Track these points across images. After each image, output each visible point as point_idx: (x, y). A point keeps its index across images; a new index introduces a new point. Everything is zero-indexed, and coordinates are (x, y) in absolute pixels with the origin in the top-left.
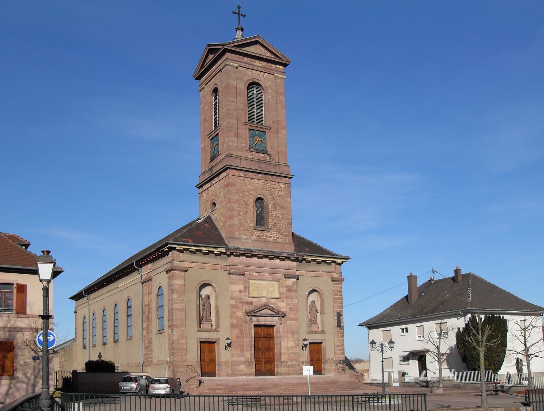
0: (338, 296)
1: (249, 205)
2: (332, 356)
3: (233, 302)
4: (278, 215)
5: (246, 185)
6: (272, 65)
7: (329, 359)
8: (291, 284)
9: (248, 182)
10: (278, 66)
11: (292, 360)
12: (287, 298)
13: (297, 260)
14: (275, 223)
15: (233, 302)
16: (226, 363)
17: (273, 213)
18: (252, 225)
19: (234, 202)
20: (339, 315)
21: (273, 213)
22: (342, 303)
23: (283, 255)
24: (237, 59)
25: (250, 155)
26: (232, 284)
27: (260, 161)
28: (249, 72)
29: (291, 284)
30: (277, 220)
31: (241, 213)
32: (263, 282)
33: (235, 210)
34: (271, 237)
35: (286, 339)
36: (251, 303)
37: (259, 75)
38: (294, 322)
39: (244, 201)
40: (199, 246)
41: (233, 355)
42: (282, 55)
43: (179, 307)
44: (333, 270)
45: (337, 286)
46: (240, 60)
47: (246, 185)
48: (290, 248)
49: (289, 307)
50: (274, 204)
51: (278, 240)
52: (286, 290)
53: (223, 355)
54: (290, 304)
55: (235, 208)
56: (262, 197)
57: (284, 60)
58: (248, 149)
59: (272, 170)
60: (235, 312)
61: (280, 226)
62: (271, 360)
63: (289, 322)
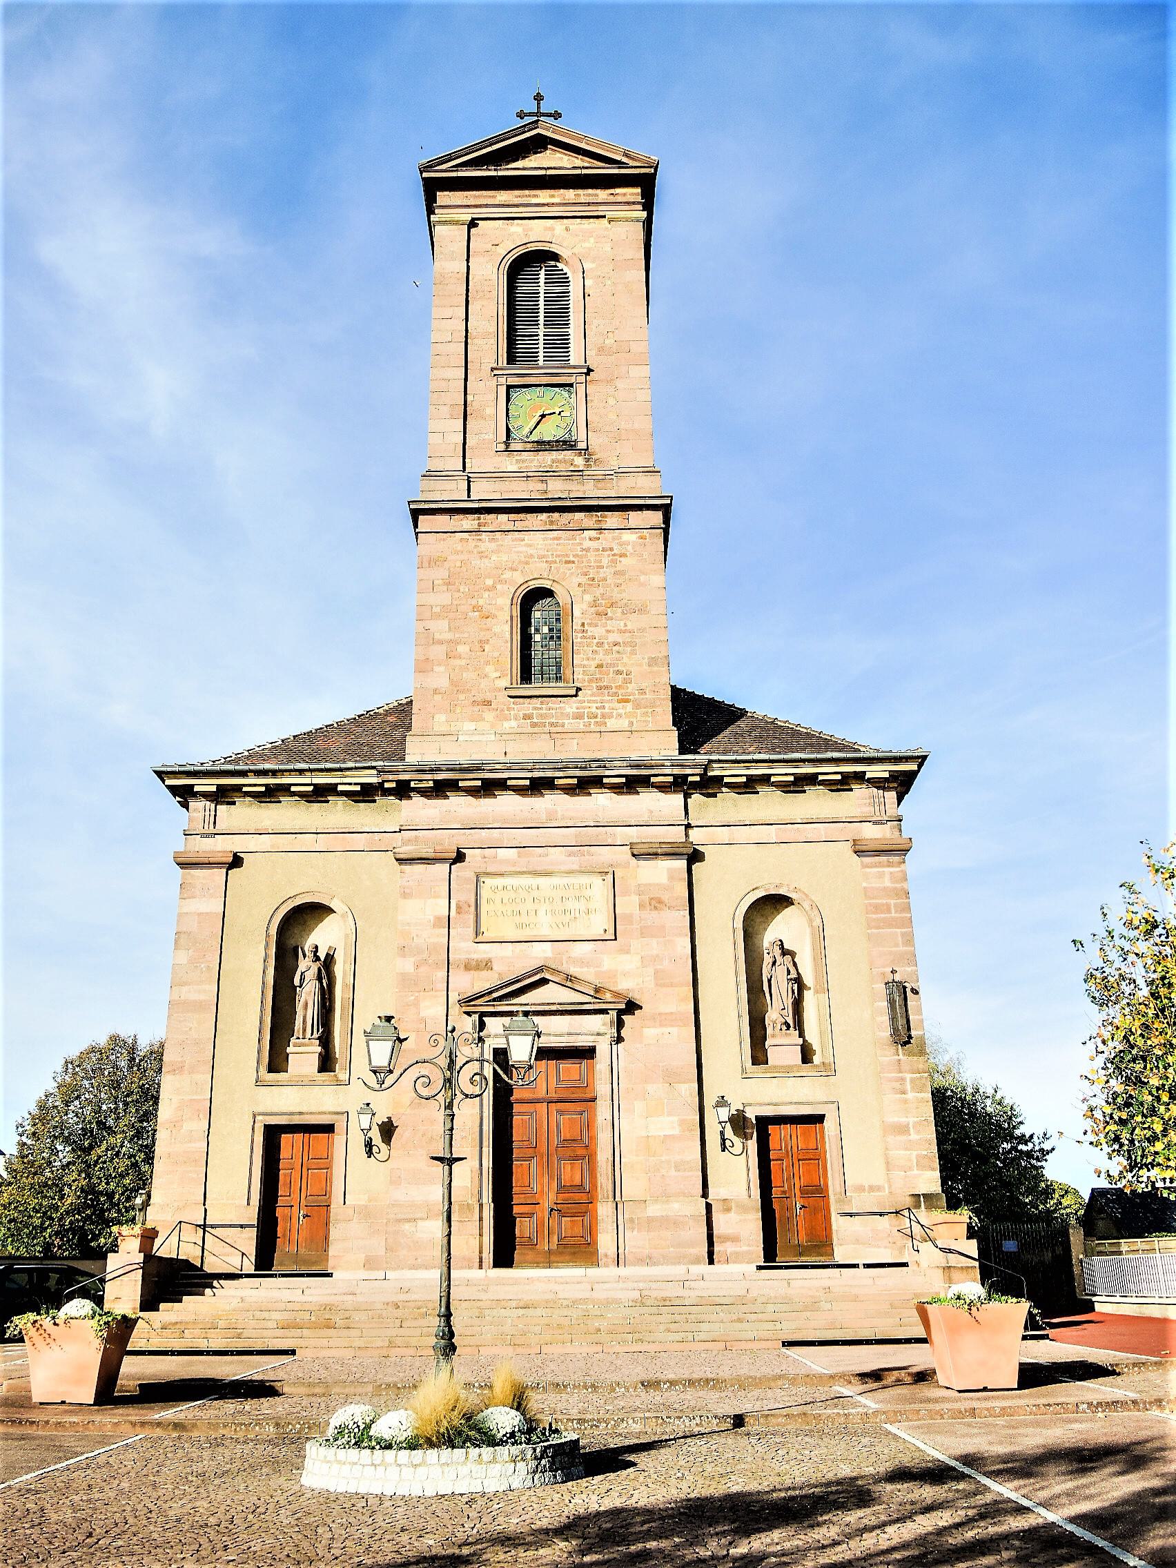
0: (894, 913)
1: (495, 616)
2: (877, 1176)
3: (407, 965)
4: (613, 638)
5: (482, 555)
6: (598, 191)
7: (860, 1189)
8: (664, 879)
9: (493, 546)
10: (618, 191)
11: (666, 1196)
12: (643, 935)
13: (679, 784)
14: (600, 666)
15: (407, 965)
16: (365, 1213)
17: (598, 631)
18: (505, 682)
19: (437, 616)
20: (900, 996)
21: (591, 631)
22: (909, 940)
23: (614, 774)
24: (517, 201)
25: (509, 464)
26: (405, 895)
27: (545, 475)
28: (516, 228)
29: (664, 879)
30: (607, 652)
31: (462, 649)
32: (542, 881)
33: (441, 642)
34: (579, 716)
35: (639, 1106)
36: (487, 965)
37: (552, 229)
38: (674, 1030)
39: (476, 608)
40: (274, 773)
41: (395, 1181)
42: (626, 155)
43: (194, 996)
44: (866, 811)
45: (881, 873)
46: (490, 202)
47: (482, 555)
48: (660, 744)
49: (651, 971)
50: (595, 603)
51: (612, 724)
52: (641, 906)
53: (357, 1179)
54: (656, 959)
55: (437, 636)
56: (547, 584)
57: (631, 163)
58: (502, 447)
59: (589, 491)
60: (416, 1004)
61: (619, 672)
62: (583, 1198)
63: (651, 1032)
